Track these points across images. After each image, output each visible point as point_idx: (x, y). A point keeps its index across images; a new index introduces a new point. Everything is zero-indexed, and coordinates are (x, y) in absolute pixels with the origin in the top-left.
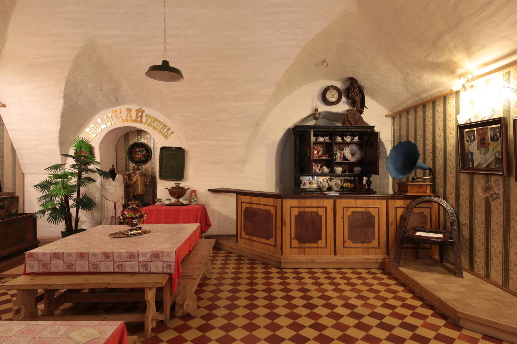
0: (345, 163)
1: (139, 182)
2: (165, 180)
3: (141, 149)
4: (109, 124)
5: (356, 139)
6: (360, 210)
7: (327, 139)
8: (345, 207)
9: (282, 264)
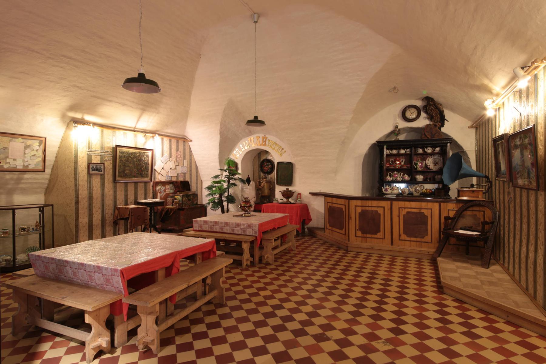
0: (426, 171)
1: (266, 187)
2: (280, 185)
3: (268, 164)
4: (246, 148)
5: (438, 149)
6: (414, 210)
7: (408, 151)
8: (401, 208)
9: (349, 248)
